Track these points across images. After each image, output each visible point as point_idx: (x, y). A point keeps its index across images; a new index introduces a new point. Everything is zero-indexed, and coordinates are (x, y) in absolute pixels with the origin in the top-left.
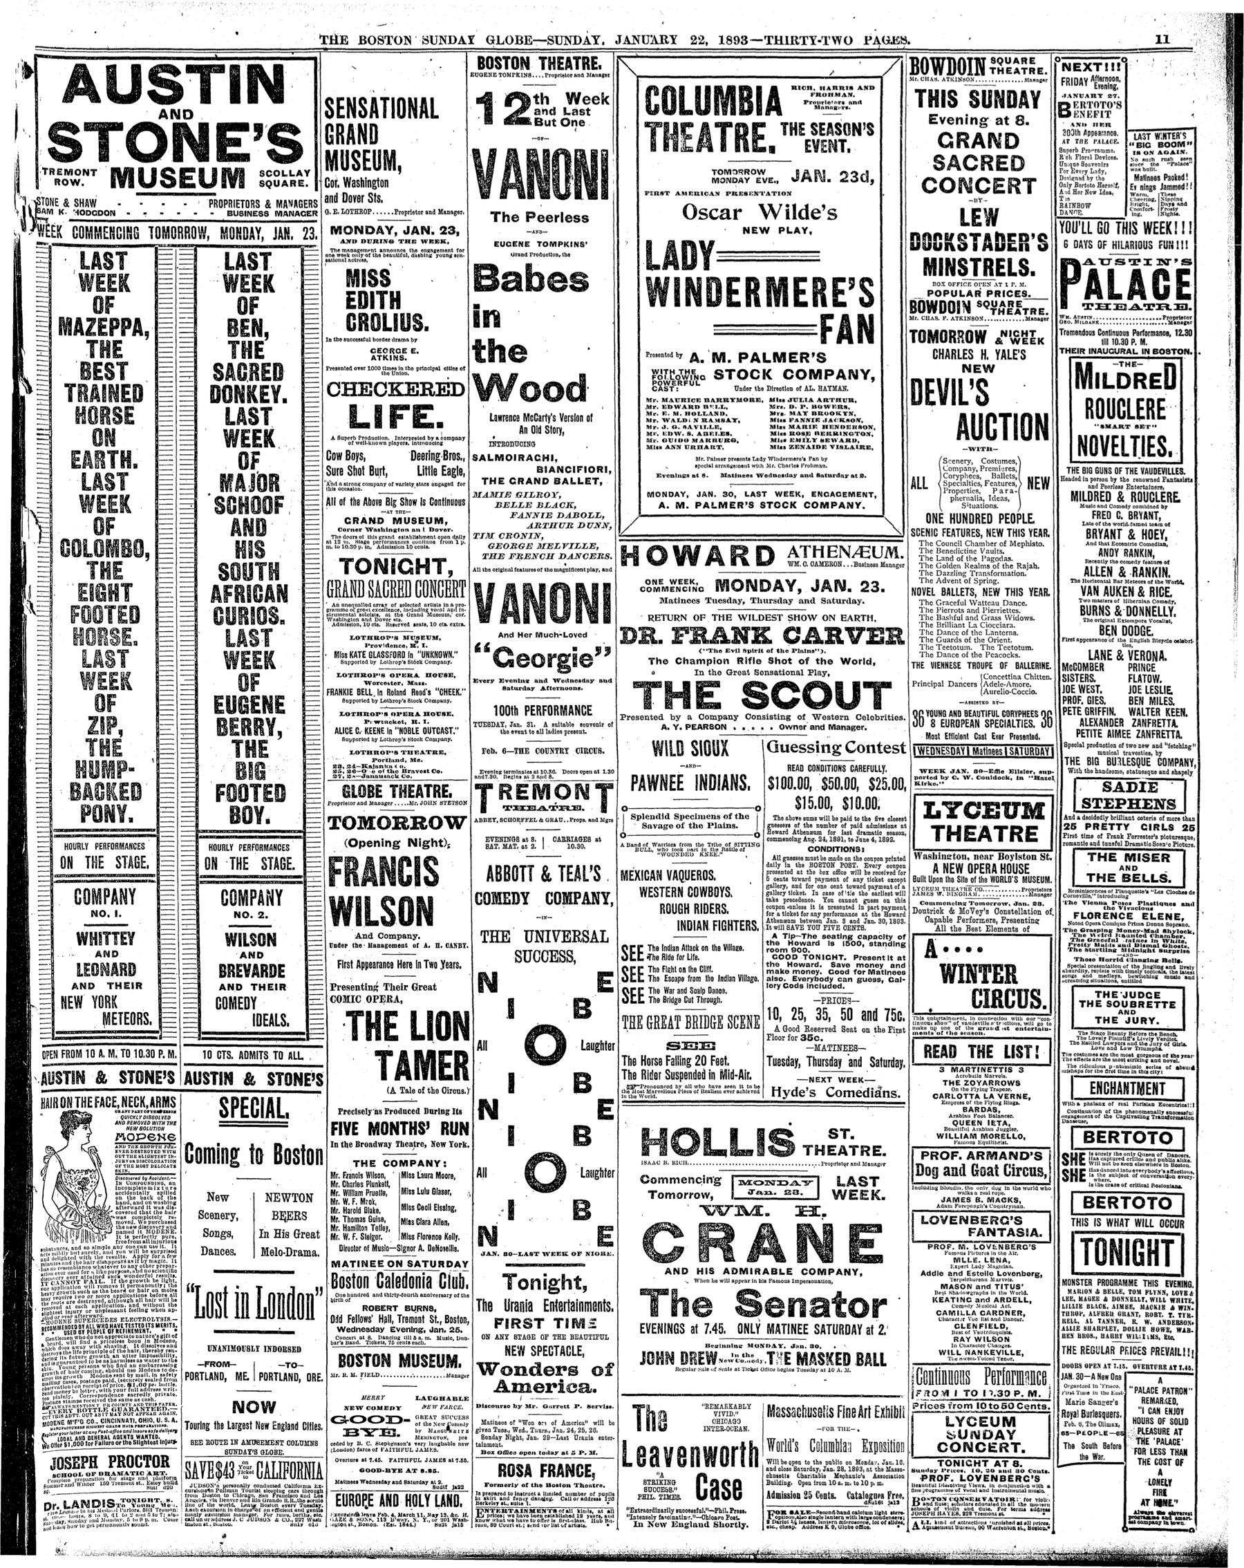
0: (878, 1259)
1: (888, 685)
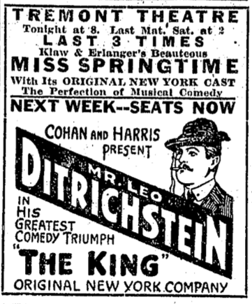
0: (86, 128)
1: (151, 147)
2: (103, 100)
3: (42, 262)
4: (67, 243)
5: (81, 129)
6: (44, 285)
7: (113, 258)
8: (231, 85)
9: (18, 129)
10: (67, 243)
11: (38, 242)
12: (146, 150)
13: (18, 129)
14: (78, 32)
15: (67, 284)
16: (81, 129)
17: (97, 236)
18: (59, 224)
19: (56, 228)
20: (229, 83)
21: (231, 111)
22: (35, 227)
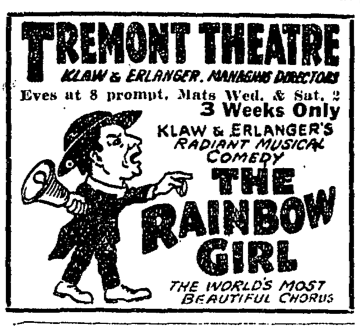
12: (172, 39)
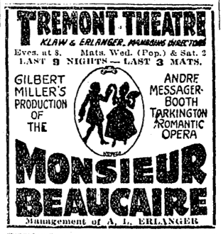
2: (118, 159)
3: (193, 102)
4: (31, 130)
5: (173, 75)
6: (191, 113)
7: (177, 110)
8: (147, 63)
9: (17, 140)
10: (31, 130)
11: (157, 94)
13: (17, 140)
14: (190, 55)
15: (193, 133)
16: (173, 75)
17: (156, 87)
18: (163, 88)
19: (161, 92)
20: (145, 62)
21: (152, 87)
22: (45, 94)
